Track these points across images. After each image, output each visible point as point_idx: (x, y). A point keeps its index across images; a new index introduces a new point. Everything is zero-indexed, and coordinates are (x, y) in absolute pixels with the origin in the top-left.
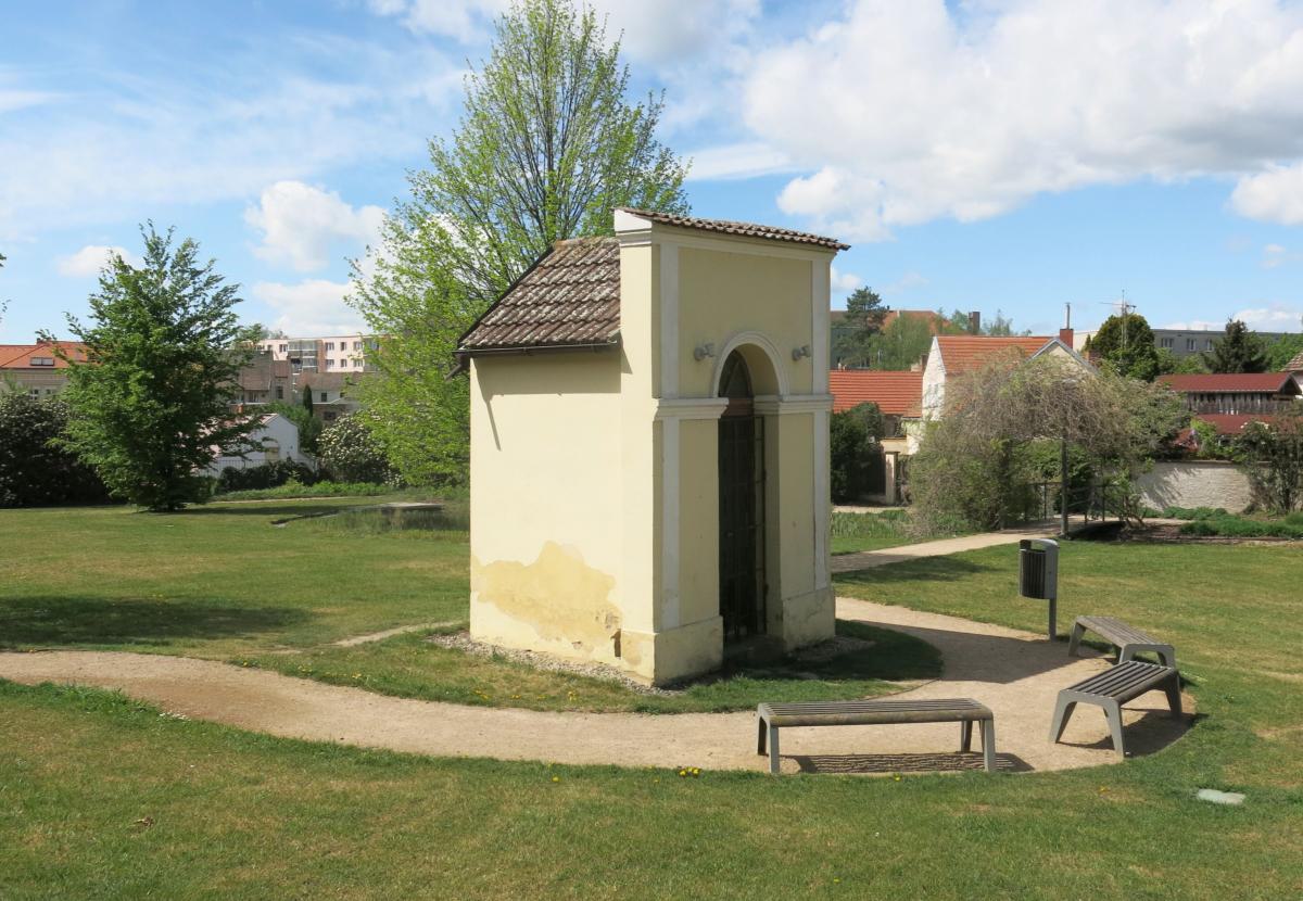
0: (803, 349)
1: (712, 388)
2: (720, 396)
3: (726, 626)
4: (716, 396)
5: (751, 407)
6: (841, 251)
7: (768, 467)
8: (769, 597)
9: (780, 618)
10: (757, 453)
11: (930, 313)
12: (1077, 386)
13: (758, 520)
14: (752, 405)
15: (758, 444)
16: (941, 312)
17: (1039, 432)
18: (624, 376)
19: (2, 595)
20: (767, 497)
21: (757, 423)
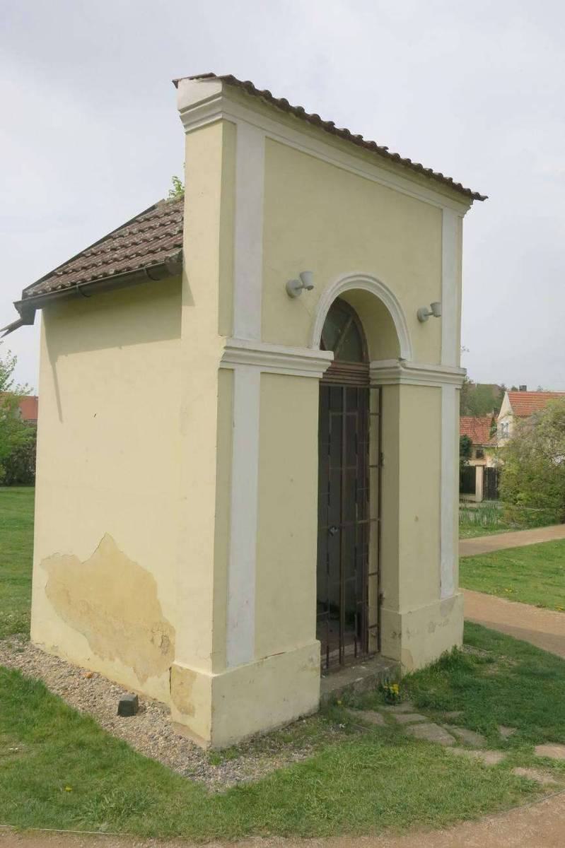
0: (432, 305)
1: (310, 336)
2: (322, 348)
3: (326, 650)
4: (317, 347)
5: (366, 375)
6: (476, 202)
7: (385, 451)
8: (384, 609)
9: (397, 635)
10: (372, 430)
11: (496, 385)
12: (322, 716)
13: (373, 513)
14: (367, 373)
15: (373, 419)
16: (503, 386)
17: (244, 793)
18: (186, 310)
19: (555, 752)
20: (377, 481)
21: (374, 393)
